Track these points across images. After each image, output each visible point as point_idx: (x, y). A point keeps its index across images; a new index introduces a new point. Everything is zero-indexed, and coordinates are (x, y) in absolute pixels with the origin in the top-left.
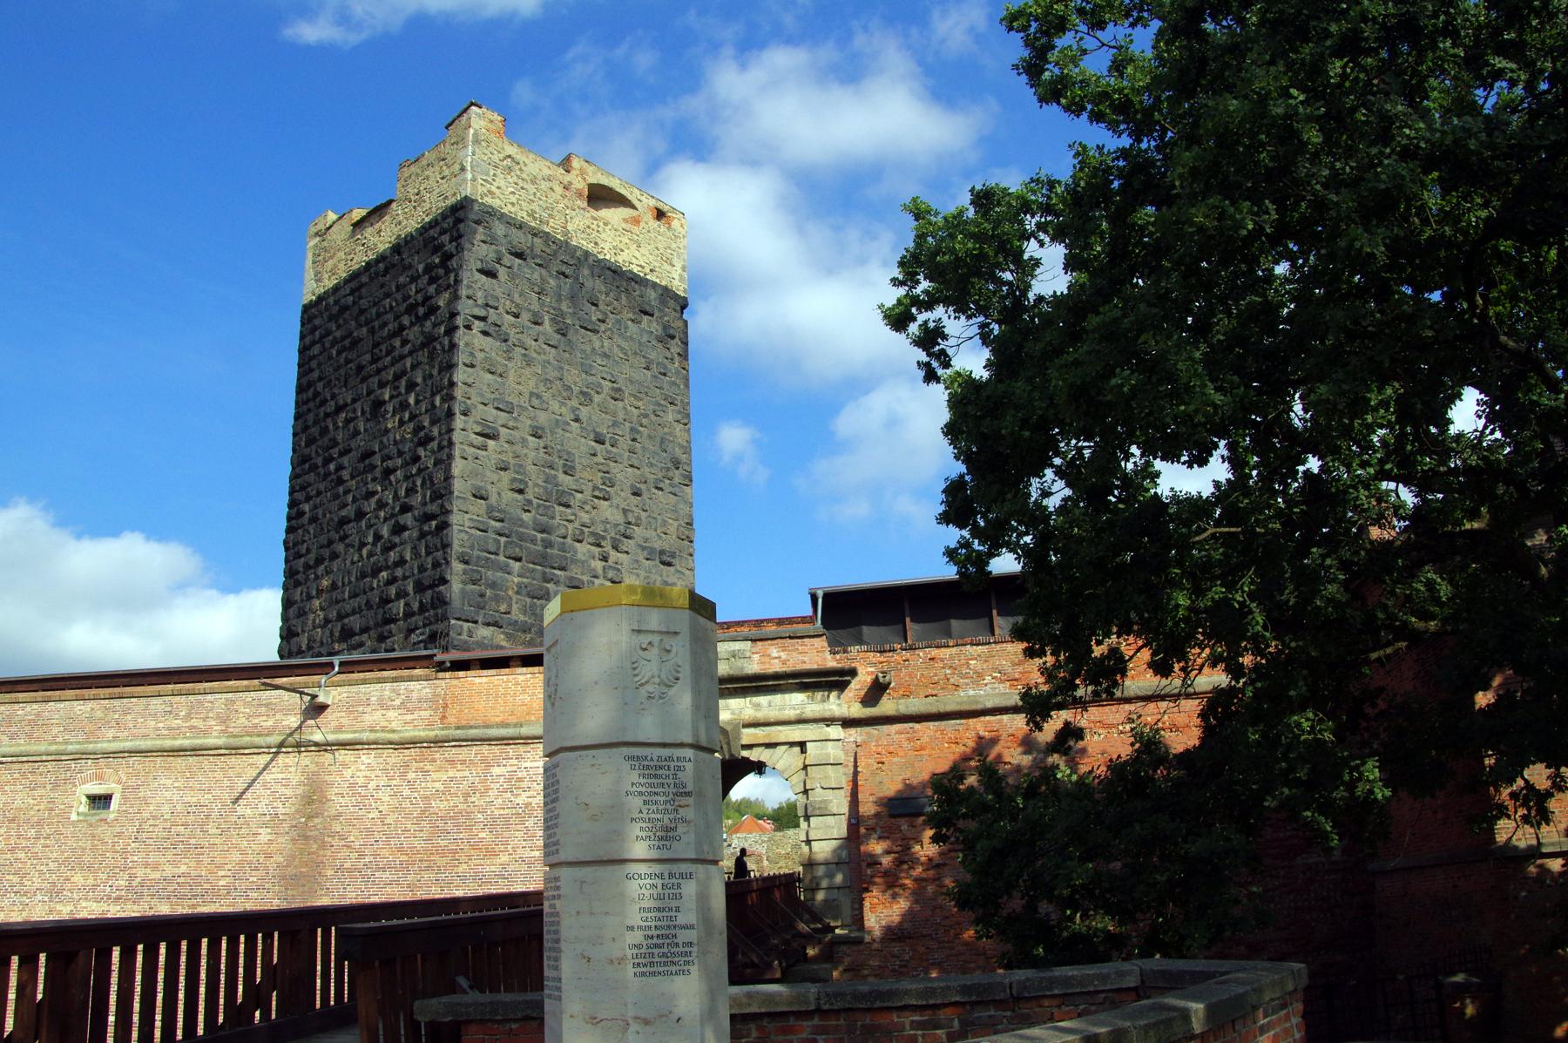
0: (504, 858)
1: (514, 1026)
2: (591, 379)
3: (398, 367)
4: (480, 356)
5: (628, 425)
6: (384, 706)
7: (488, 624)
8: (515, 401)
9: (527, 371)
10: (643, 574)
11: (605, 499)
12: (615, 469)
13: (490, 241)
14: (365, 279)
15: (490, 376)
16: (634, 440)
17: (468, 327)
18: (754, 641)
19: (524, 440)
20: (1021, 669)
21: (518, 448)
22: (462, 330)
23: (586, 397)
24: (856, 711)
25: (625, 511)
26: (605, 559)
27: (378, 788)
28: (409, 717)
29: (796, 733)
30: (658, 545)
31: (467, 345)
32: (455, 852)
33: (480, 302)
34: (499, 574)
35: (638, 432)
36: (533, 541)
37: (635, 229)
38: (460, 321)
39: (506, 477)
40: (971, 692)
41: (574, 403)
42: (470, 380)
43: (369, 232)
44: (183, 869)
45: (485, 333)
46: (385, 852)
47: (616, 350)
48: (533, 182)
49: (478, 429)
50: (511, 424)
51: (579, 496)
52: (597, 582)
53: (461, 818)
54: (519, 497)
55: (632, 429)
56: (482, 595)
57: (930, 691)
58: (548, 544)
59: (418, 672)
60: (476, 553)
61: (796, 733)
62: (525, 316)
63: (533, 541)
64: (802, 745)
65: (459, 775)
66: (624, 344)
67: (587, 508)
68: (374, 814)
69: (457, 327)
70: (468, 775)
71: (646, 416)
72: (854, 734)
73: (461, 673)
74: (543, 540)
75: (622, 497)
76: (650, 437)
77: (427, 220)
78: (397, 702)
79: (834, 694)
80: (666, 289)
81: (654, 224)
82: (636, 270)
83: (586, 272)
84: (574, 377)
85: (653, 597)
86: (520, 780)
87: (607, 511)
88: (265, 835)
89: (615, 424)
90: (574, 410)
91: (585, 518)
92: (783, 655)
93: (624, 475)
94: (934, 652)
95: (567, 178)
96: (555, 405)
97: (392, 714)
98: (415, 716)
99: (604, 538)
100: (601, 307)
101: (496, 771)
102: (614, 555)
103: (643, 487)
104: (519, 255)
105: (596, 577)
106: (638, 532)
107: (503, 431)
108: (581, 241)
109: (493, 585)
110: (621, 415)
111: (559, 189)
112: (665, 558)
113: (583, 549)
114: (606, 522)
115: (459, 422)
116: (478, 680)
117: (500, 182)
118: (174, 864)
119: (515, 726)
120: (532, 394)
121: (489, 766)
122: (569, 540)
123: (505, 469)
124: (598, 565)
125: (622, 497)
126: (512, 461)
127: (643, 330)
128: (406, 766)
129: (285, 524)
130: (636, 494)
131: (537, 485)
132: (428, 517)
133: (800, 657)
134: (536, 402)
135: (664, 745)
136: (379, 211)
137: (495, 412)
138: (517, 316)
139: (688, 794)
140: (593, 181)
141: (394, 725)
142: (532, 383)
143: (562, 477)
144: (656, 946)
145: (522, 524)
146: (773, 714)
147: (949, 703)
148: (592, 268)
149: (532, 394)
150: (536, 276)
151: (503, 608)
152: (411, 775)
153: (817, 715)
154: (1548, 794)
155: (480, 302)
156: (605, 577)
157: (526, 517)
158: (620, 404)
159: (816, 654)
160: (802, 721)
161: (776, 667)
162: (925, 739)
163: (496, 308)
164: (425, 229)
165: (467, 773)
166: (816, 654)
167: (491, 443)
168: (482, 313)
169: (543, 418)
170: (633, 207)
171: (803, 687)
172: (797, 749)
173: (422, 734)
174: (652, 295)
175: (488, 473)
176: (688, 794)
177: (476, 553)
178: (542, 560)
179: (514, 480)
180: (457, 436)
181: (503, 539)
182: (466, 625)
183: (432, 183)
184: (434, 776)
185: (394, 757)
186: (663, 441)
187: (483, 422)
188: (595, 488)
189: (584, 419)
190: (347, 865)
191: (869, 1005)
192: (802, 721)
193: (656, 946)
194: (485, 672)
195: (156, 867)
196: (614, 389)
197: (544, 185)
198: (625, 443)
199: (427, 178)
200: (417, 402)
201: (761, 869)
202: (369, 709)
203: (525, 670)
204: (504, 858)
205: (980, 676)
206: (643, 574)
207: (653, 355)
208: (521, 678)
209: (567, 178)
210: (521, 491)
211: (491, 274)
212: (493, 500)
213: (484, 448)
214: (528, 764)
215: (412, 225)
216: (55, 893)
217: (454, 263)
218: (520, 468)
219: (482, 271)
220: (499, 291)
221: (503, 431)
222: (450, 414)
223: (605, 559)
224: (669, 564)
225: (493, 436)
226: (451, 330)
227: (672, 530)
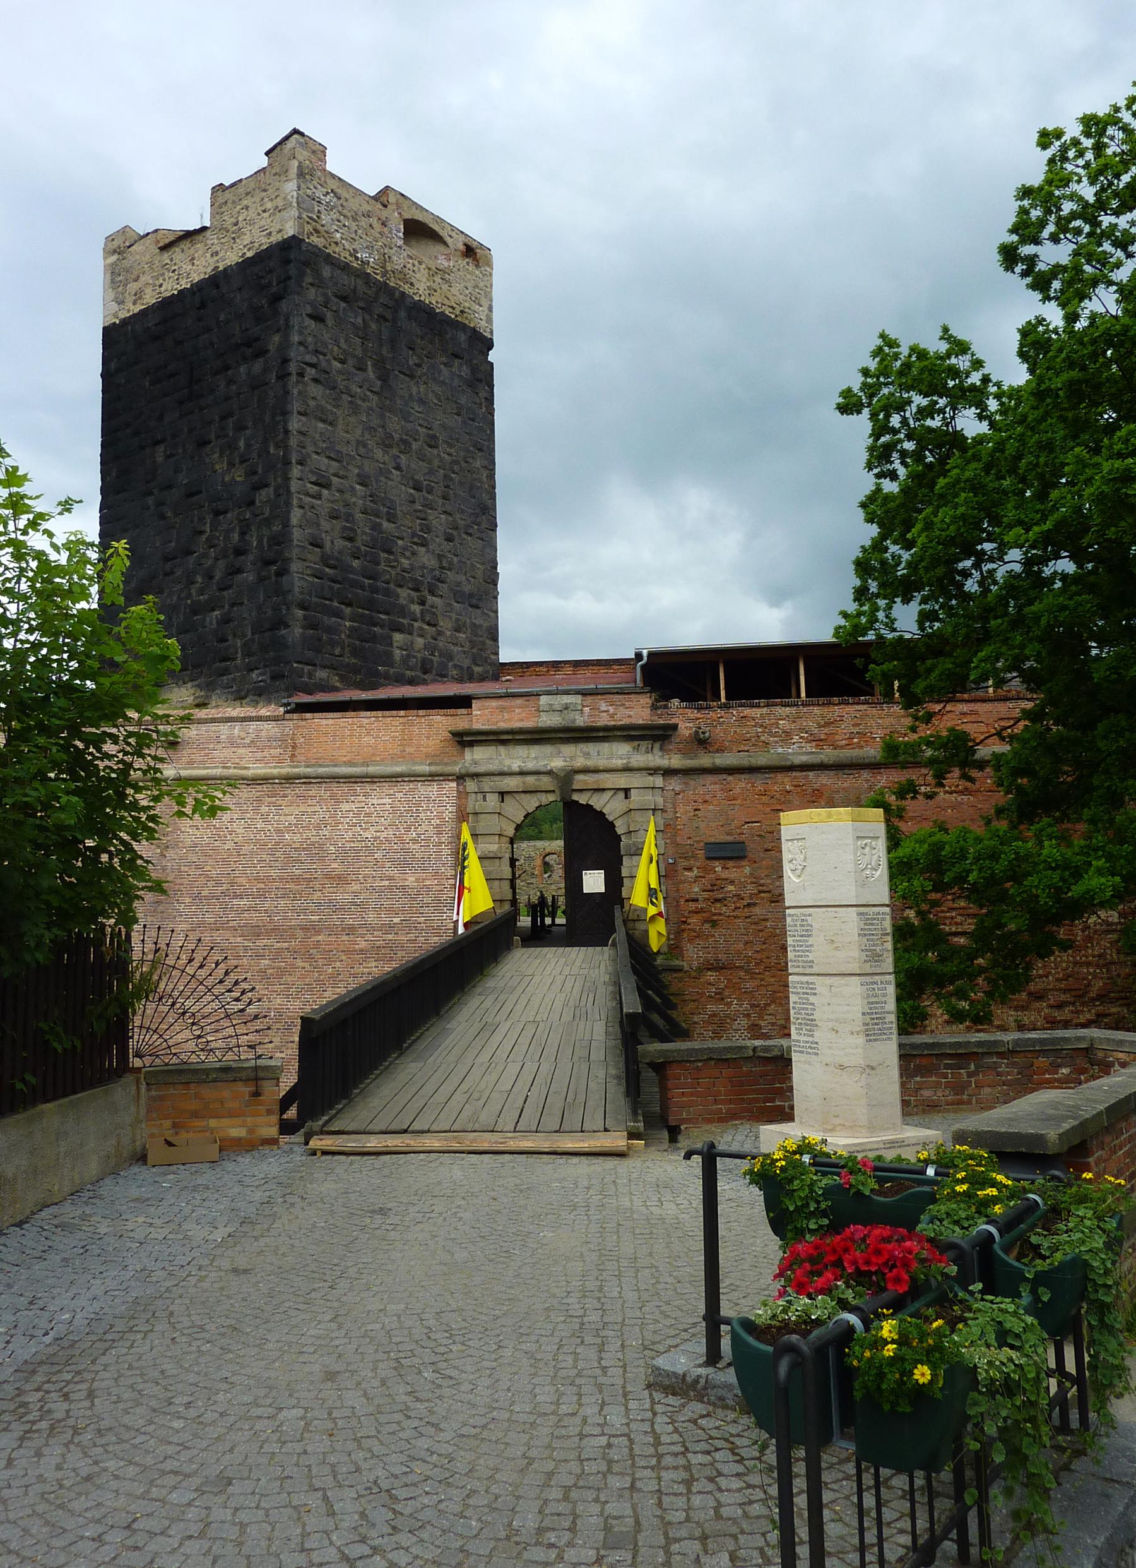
0: (356, 887)
1: (700, 1064)
2: (409, 426)
4: (312, 403)
5: (442, 471)
6: (232, 743)
7: (325, 667)
8: (344, 450)
9: (352, 419)
10: (454, 616)
11: (422, 545)
12: (432, 515)
13: (319, 284)
15: (321, 425)
16: (447, 487)
17: (301, 375)
18: (584, 693)
19: (353, 489)
20: (826, 730)
21: (347, 496)
22: (294, 378)
23: (405, 445)
24: (676, 761)
25: (440, 557)
26: (422, 603)
27: (232, 821)
28: (259, 755)
29: (622, 781)
30: (467, 589)
31: (300, 393)
32: (310, 880)
33: (311, 348)
34: (334, 619)
35: (451, 479)
36: (363, 588)
38: (293, 368)
39: (338, 525)
40: (780, 750)
41: (395, 451)
42: (304, 429)
45: (316, 380)
46: (243, 881)
47: (431, 395)
48: (355, 219)
49: (314, 479)
50: (341, 473)
51: (400, 542)
52: (416, 624)
53: (316, 850)
54: (349, 545)
55: (445, 476)
56: (320, 640)
57: (742, 748)
58: (374, 590)
59: (264, 712)
60: (315, 599)
61: (622, 781)
62: (351, 362)
63: (363, 588)
64: (627, 791)
65: (310, 809)
66: (437, 389)
67: (408, 554)
68: (230, 845)
69: (290, 374)
70: (321, 812)
71: (456, 462)
72: (675, 784)
73: (308, 715)
74: (370, 585)
75: (438, 543)
76: (461, 483)
77: (249, 254)
78: (247, 741)
79: (657, 745)
83: (402, 314)
86: (369, 815)
87: (425, 558)
89: (431, 472)
90: (396, 457)
91: (405, 563)
92: (611, 709)
93: (439, 521)
94: (747, 711)
95: (385, 213)
96: (379, 454)
98: (266, 754)
99: (422, 583)
100: (418, 351)
101: (345, 806)
102: (431, 599)
103: (455, 533)
104: (344, 299)
105: (416, 620)
106: (451, 575)
107: (335, 480)
109: (329, 630)
110: (436, 463)
112: (474, 601)
113: (404, 593)
114: (423, 567)
115: (296, 471)
116: (324, 722)
119: (363, 765)
120: (358, 442)
121: (338, 802)
122: (392, 586)
123: (336, 518)
124: (416, 608)
125: (438, 543)
126: (343, 510)
127: (453, 373)
128: (259, 800)
130: (449, 539)
131: (364, 533)
132: (268, 563)
133: (627, 712)
134: (362, 451)
135: (874, 906)
137: (326, 461)
138: (342, 362)
139: (887, 934)
140: (407, 216)
141: (243, 763)
142: (359, 432)
143: (385, 525)
144: (876, 1024)
146: (602, 763)
147: (761, 760)
149: (358, 442)
150: (360, 320)
151: (337, 651)
152: (264, 809)
153: (642, 765)
155: (311, 348)
156: (423, 621)
157: (356, 563)
158: (435, 451)
159: (638, 710)
160: (627, 769)
161: (604, 720)
162: (737, 791)
163: (325, 355)
164: (246, 264)
165: (317, 808)
166: (638, 710)
167: (325, 492)
168: (314, 360)
169: (368, 467)
170: (445, 243)
171: (629, 738)
172: (622, 795)
173: (275, 771)
174: (462, 337)
175: (322, 522)
176: (887, 934)
177: (315, 599)
178: (370, 605)
179: (345, 528)
180: (294, 486)
181: (337, 586)
182: (307, 668)
184: (287, 810)
186: (472, 487)
187: (317, 471)
188: (414, 535)
189: (404, 468)
190: (204, 893)
191: (920, 1052)
192: (627, 769)
193: (876, 1024)
194: (331, 715)
196: (429, 436)
197: (364, 222)
198: (439, 489)
199: (247, 208)
200: (248, 445)
201: (204, 797)
202: (219, 746)
203: (368, 713)
204: (356, 887)
205: (788, 734)
206: (454, 616)
207: (463, 401)
208: (365, 721)
209: (385, 213)
210: (351, 539)
211: (318, 318)
212: (328, 545)
213: (318, 497)
214: (375, 802)
215: (232, 258)
217: (284, 306)
218: (349, 517)
219: (310, 316)
220: (326, 337)
221: (335, 480)
222: (287, 463)
223: (422, 603)
224: (477, 607)
225: (327, 486)
226: (283, 376)
227: (479, 574)
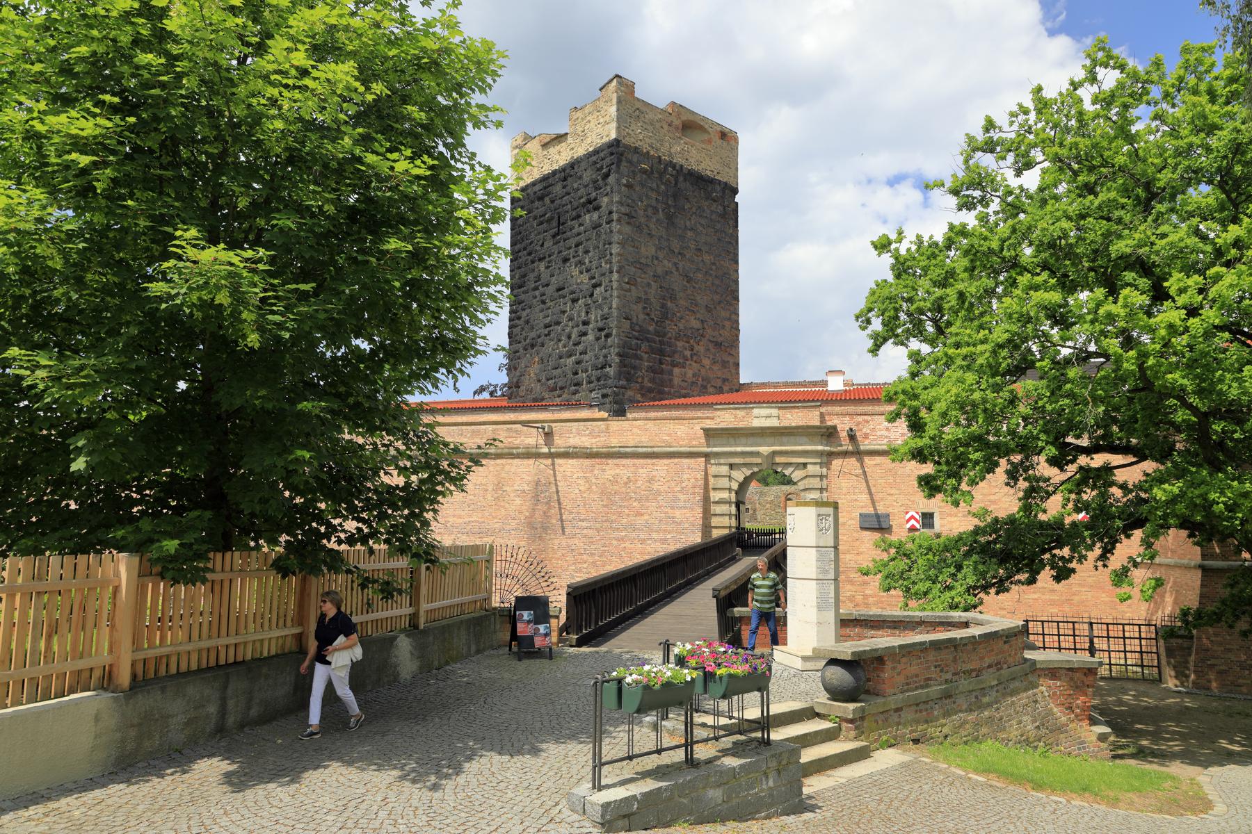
0: (646, 517)
3: (577, 239)
14: (550, 181)
37: (709, 147)
39: (640, 306)
43: (552, 150)
44: (475, 518)
80: (726, 184)
81: (719, 142)
82: (709, 173)
84: (676, 245)
85: (819, 504)
88: (518, 501)
97: (584, 439)
108: (678, 160)
111: (666, 127)
117: (633, 127)
118: (469, 515)
124: (688, 353)
129: (508, 323)
136: (560, 138)
145: (649, 332)
148: (685, 175)
152: (596, 472)
154: (403, 631)
169: (660, 271)
183: (592, 125)
185: (587, 462)
195: (460, 517)
197: (658, 125)
213: (630, 290)
215: (581, 151)
216: (664, 540)
